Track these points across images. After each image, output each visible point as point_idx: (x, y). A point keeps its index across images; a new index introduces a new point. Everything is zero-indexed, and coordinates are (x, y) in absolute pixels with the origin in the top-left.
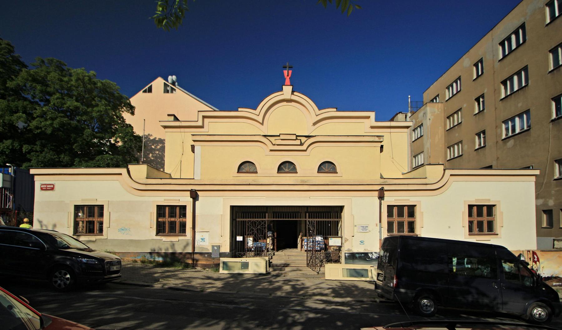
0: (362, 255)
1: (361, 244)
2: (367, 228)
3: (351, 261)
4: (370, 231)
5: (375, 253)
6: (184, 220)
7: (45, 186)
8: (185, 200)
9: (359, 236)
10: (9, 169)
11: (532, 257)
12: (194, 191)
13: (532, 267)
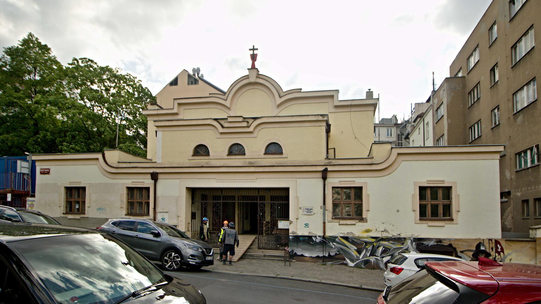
0: (306, 238)
1: (306, 226)
2: (311, 210)
4: (315, 214)
5: (319, 236)
8: (148, 182)
9: (304, 219)
10: (27, 157)
11: (494, 247)
12: (155, 174)
13: (495, 258)
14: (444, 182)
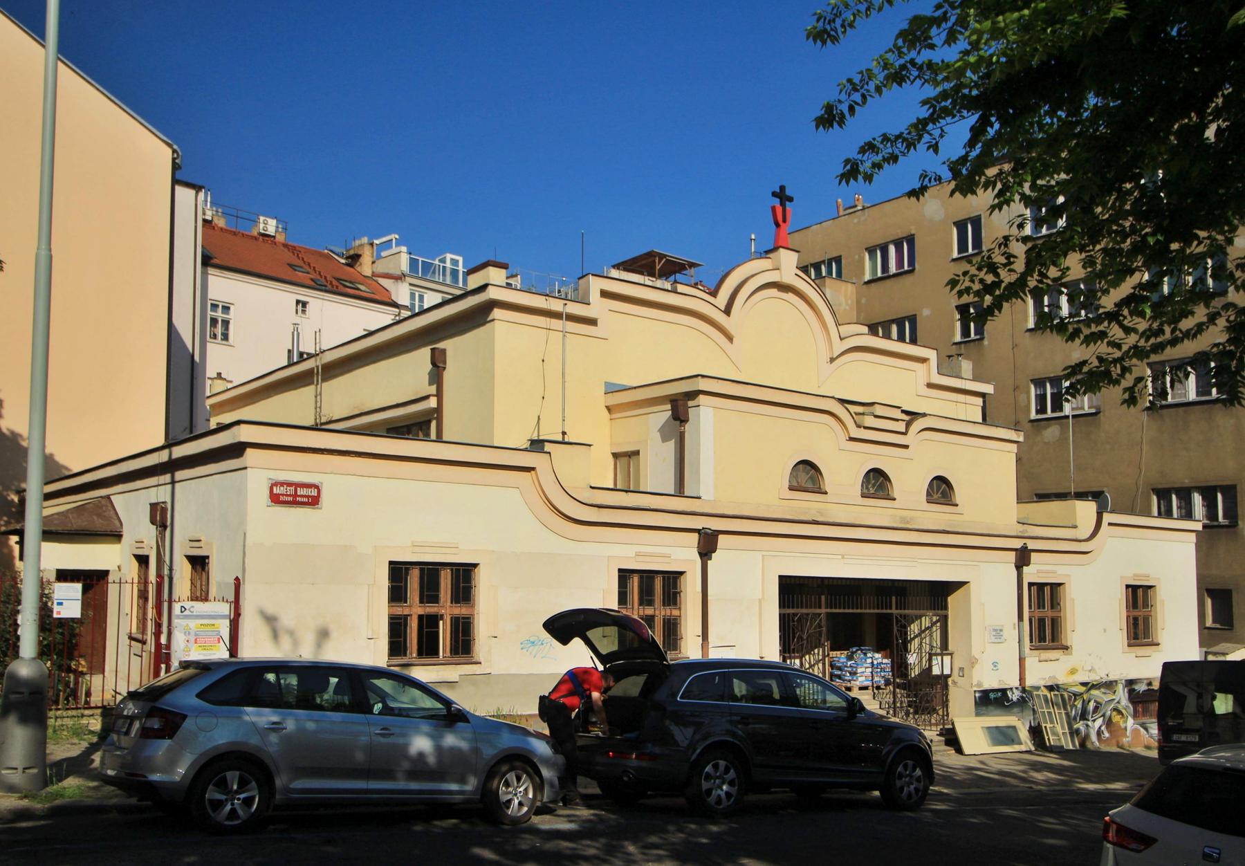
2: (1001, 633)
3: (984, 708)
6: (675, 613)
7: (291, 490)
14: (1147, 579)
